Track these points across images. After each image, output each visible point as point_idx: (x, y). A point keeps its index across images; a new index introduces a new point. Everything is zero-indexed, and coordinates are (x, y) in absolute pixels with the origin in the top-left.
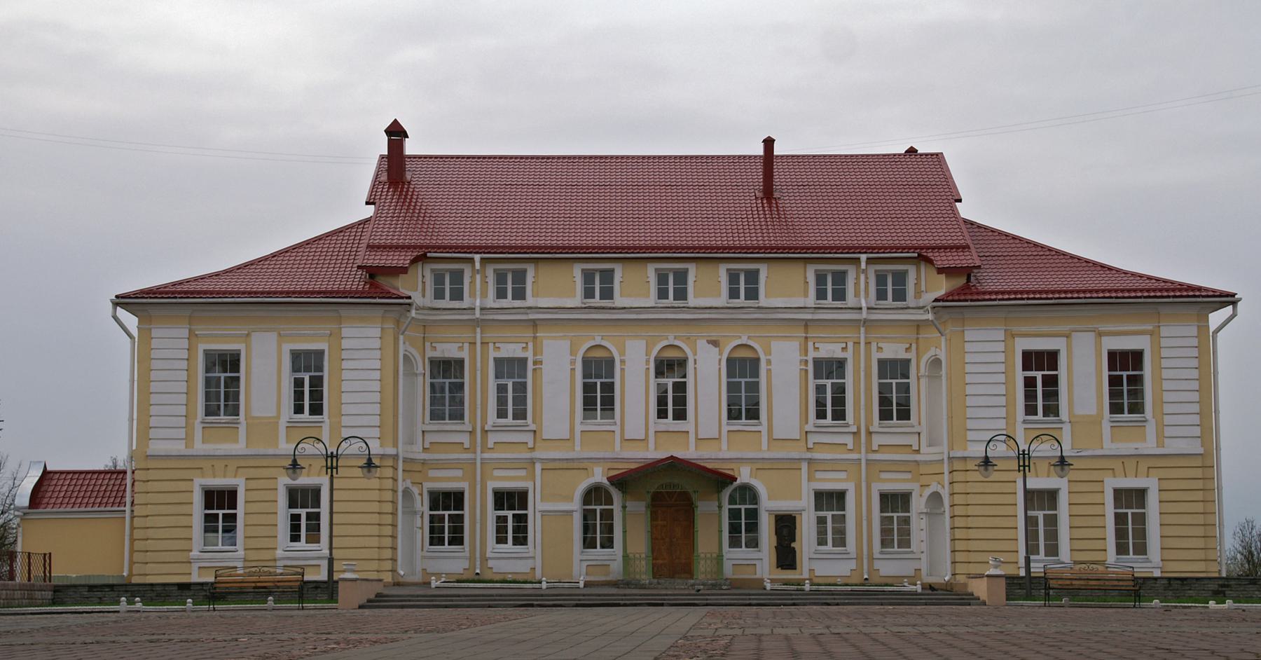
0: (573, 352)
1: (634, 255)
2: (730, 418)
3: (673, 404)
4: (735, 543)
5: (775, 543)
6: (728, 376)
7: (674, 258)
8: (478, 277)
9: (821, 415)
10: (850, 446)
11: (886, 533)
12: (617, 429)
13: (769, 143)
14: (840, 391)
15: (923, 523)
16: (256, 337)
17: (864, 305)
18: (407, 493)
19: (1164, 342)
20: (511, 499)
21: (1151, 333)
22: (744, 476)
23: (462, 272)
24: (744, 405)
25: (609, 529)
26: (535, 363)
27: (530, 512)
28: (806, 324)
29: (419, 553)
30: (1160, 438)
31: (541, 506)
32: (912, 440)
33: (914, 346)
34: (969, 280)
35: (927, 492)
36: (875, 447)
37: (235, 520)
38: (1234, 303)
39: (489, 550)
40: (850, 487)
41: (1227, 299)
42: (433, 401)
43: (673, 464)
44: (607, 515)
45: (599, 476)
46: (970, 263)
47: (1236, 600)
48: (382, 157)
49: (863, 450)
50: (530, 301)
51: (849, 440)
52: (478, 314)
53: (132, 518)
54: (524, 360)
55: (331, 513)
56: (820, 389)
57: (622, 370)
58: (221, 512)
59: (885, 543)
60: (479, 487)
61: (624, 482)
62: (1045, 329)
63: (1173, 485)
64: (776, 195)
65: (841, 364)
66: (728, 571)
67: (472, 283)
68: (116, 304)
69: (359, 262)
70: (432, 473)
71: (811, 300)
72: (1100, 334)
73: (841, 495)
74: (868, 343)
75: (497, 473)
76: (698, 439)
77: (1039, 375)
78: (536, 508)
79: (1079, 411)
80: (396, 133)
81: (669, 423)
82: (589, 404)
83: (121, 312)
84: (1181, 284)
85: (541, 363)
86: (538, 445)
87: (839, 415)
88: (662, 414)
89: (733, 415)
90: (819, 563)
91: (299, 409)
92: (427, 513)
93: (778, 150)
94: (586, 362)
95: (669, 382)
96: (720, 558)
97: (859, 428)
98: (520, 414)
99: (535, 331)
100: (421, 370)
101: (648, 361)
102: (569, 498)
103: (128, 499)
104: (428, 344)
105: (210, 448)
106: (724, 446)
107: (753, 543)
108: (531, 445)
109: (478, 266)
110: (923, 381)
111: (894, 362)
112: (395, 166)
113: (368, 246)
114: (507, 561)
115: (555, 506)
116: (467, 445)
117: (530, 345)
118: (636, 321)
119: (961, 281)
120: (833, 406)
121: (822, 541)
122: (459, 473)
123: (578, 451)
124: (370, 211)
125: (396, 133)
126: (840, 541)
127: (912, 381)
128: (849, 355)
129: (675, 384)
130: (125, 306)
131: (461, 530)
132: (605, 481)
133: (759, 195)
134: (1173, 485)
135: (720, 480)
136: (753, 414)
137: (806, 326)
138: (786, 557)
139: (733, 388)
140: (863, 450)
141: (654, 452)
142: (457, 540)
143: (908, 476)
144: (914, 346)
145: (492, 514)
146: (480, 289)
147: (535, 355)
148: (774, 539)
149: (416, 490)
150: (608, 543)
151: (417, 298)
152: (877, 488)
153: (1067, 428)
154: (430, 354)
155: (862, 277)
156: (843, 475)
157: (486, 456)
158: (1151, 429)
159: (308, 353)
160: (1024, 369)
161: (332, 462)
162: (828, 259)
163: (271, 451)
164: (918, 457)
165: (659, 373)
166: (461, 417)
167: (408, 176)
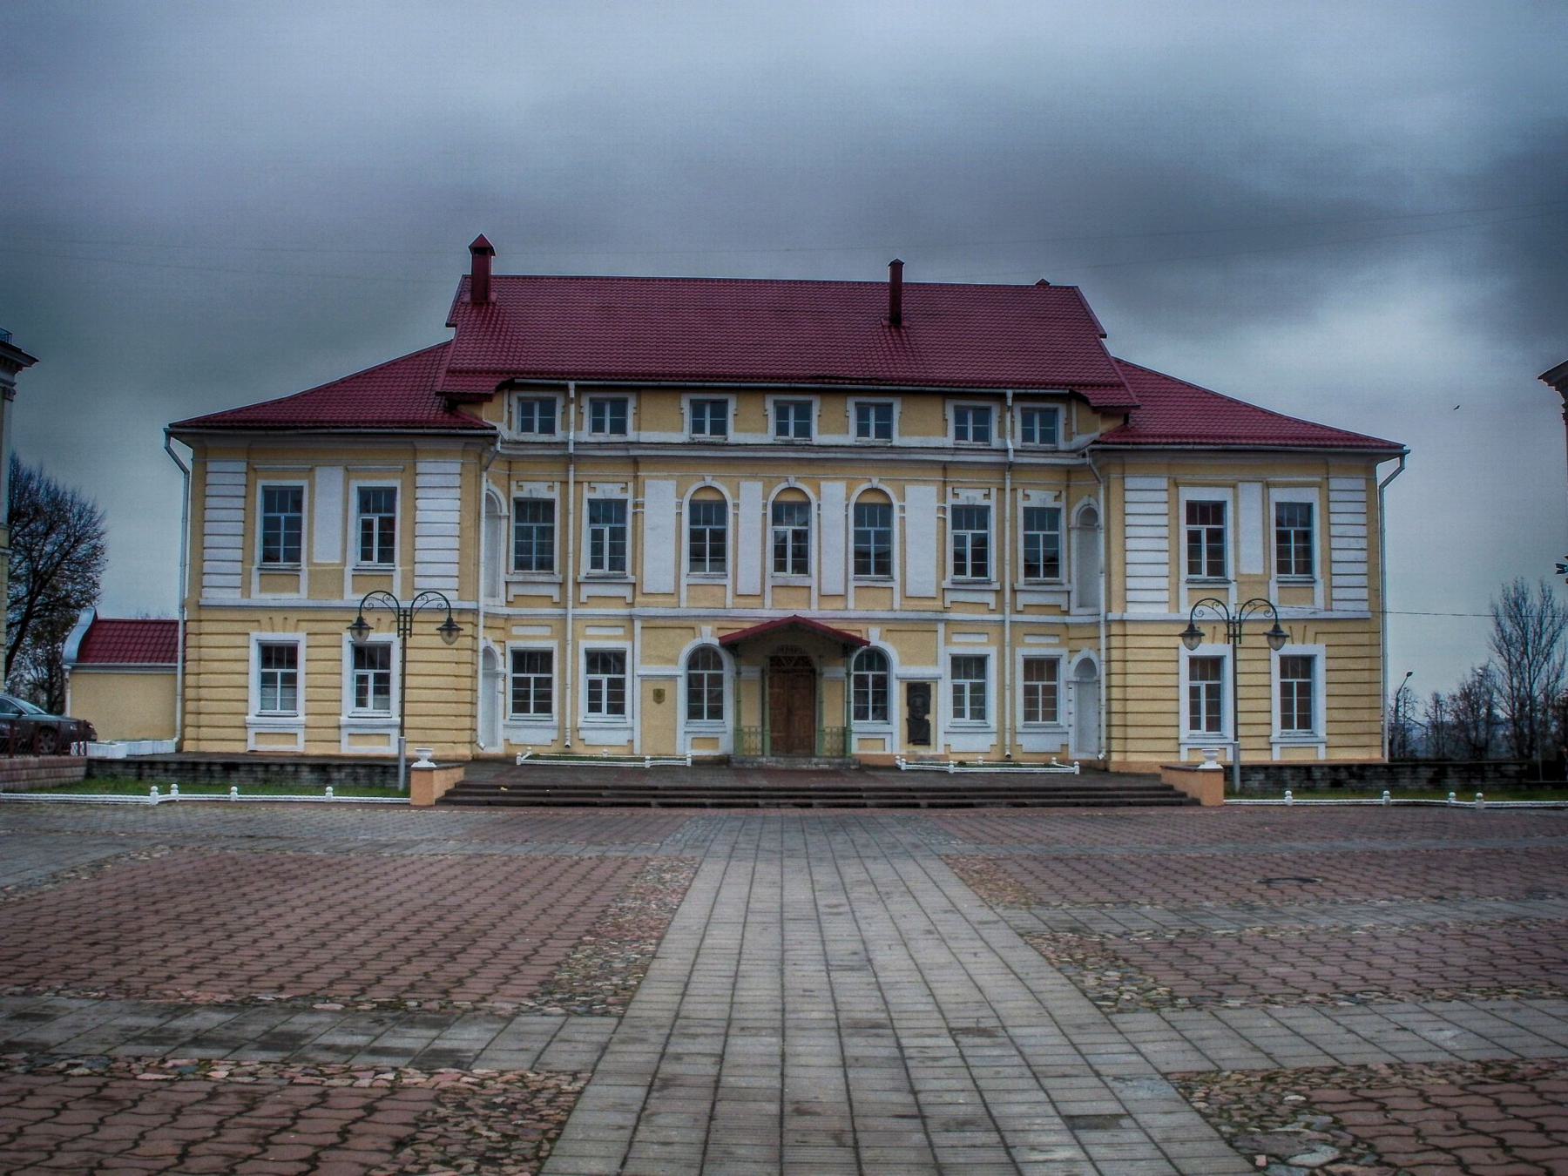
0: (680, 495)
1: (751, 386)
2: (857, 571)
3: (793, 554)
4: (861, 714)
5: (906, 715)
6: (856, 525)
7: (796, 390)
8: (573, 407)
9: (960, 569)
10: (992, 606)
11: (1030, 702)
12: (729, 582)
13: (896, 267)
14: (981, 543)
15: (1072, 694)
16: (318, 472)
17: (1010, 446)
18: (488, 653)
19: (1334, 496)
20: (605, 661)
21: (1319, 485)
22: (875, 637)
23: (553, 401)
24: (873, 557)
25: (717, 698)
26: (636, 505)
27: (628, 676)
28: (945, 466)
29: (501, 722)
30: (1330, 599)
31: (640, 671)
32: (1061, 600)
33: (1064, 494)
34: (1126, 421)
35: (1077, 659)
36: (1020, 607)
37: (388, 681)
38: (1402, 456)
39: (580, 719)
40: (992, 652)
41: (1396, 451)
42: (518, 549)
43: (795, 625)
44: (717, 681)
45: (709, 636)
46: (1124, 401)
47: (1489, 794)
48: (465, 277)
49: (1007, 610)
50: (631, 435)
51: (991, 599)
52: (571, 449)
53: (184, 674)
54: (623, 503)
55: (403, 675)
56: (960, 541)
57: (736, 515)
58: (533, 676)
59: (1030, 715)
60: (569, 648)
61: (733, 645)
62: (1211, 478)
63: (231, 694)
64: (905, 323)
65: (983, 511)
66: (856, 748)
67: (566, 413)
68: (169, 434)
69: (438, 389)
70: (516, 631)
71: (950, 441)
72: (1268, 485)
73: (981, 661)
74: (1013, 490)
75: (590, 632)
76: (821, 596)
77: (1203, 529)
78: (638, 670)
79: (1244, 570)
80: (482, 251)
81: (789, 576)
82: (697, 557)
83: (175, 444)
84: (1348, 433)
85: (643, 505)
86: (638, 599)
87: (981, 570)
88: (780, 566)
89: (862, 568)
90: (959, 743)
91: (366, 555)
92: (510, 675)
93: (907, 277)
94: (694, 506)
95: (788, 529)
96: (845, 733)
97: (1003, 586)
98: (617, 563)
99: (637, 470)
100: (505, 511)
101: (765, 506)
102: (673, 661)
103: (180, 655)
104: (513, 483)
105: (268, 598)
106: (851, 604)
107: (882, 713)
108: (629, 600)
109: (572, 394)
110: (1074, 534)
111: (1041, 511)
112: (480, 291)
113: (448, 371)
114: (605, 738)
115: (657, 664)
116: (556, 599)
117: (631, 485)
118: (750, 460)
119: (1120, 422)
120: (971, 560)
121: (959, 713)
122: (546, 631)
123: (685, 607)
124: (451, 334)
125: (482, 251)
126: (979, 713)
127: (1062, 532)
128: (992, 503)
129: (795, 533)
130: (178, 436)
131: (549, 696)
132: (716, 642)
133: (886, 323)
134: (231, 694)
135: (844, 644)
136: (884, 567)
137: (945, 469)
138: (919, 731)
139: (861, 537)
140: (1007, 610)
141: (772, 610)
142: (544, 707)
143: (1056, 640)
144: (1064, 494)
145: (583, 679)
146: (575, 426)
147: (636, 496)
148: (906, 710)
149: (497, 649)
150: (716, 713)
151: (502, 430)
152: (1022, 652)
153: (1233, 588)
154: (516, 493)
155: (1008, 415)
156: (984, 639)
157: (579, 611)
158: (1319, 589)
159: (377, 492)
160: (588, 672)
161: (405, 619)
162: (972, 398)
163: (336, 602)
164: (1068, 619)
165: (777, 519)
166: (551, 567)
167: (493, 296)
